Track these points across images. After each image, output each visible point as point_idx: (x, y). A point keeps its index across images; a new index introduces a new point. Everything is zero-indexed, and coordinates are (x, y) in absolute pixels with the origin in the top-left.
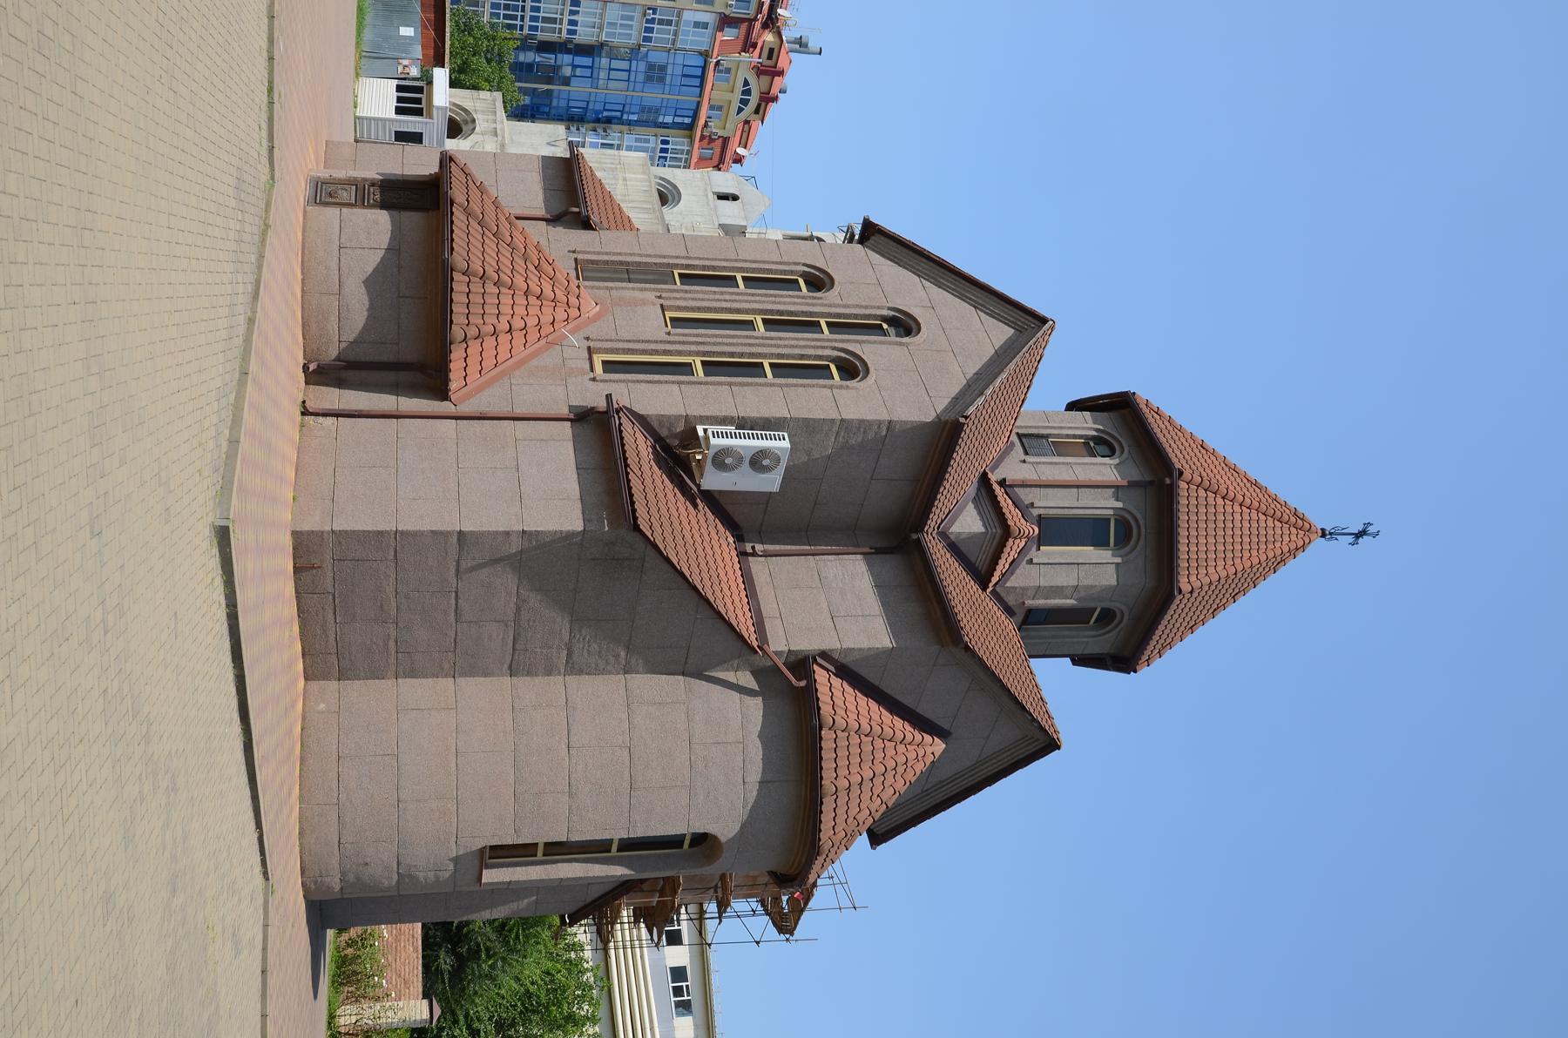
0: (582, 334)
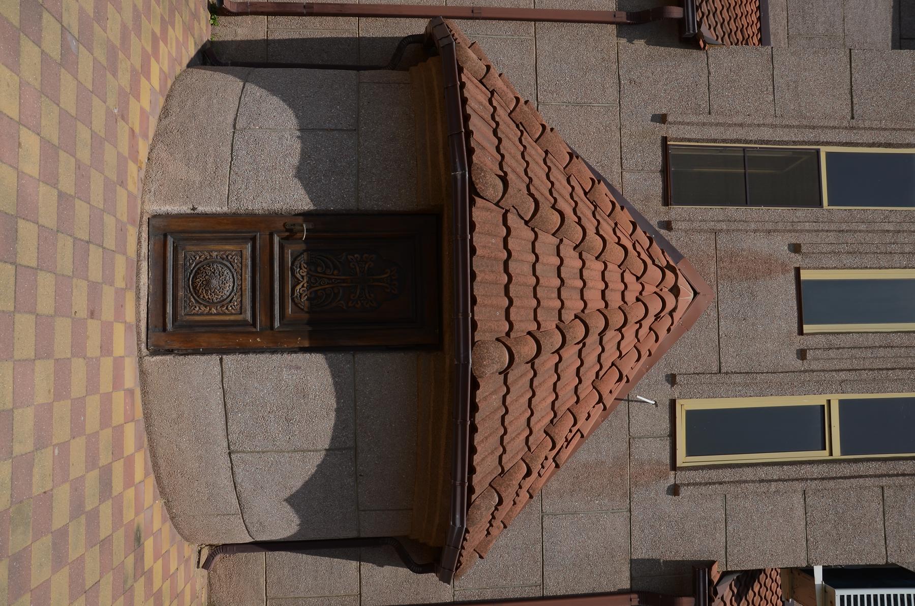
0: (659, 371)
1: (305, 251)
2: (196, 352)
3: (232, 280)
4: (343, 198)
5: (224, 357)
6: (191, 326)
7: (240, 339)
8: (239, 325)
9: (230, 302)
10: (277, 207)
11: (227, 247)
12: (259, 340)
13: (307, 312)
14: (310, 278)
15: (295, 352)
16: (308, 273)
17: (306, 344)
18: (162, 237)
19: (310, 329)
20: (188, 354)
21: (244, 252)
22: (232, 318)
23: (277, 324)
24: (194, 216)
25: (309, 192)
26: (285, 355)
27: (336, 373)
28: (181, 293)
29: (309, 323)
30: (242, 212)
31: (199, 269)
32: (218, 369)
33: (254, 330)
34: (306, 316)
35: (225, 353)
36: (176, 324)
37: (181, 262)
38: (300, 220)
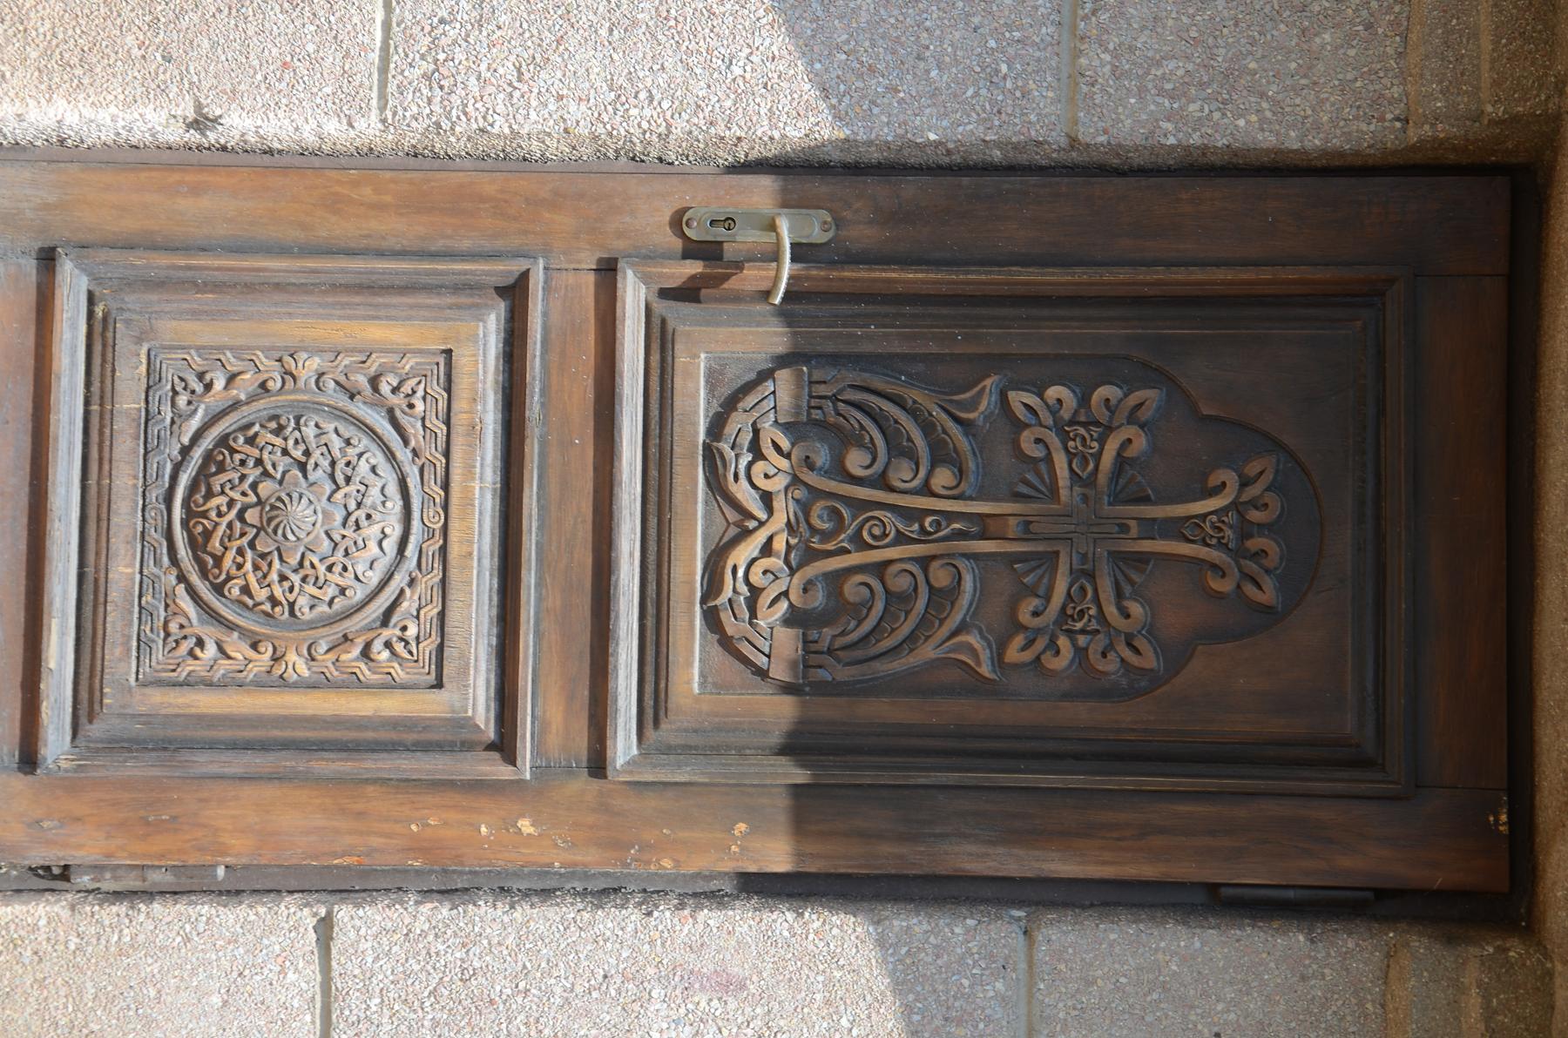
1: (783, 361)
2: (189, 885)
3: (395, 505)
4: (993, 78)
5: (344, 913)
6: (168, 743)
7: (434, 820)
8: (426, 747)
9: (386, 619)
10: (638, 122)
11: (376, 332)
12: (526, 826)
13: (788, 689)
14: (805, 508)
15: (715, 898)
16: (796, 480)
17: (777, 857)
18: (30, 266)
19: (801, 776)
20: (149, 895)
21: (462, 360)
22: (392, 705)
23: (624, 746)
24: (204, 160)
25: (811, 45)
26: (665, 915)
27: (907, 980)
28: (123, 571)
29: (795, 746)
30: (458, 145)
31: (223, 441)
32: (304, 977)
33: (504, 772)
34: (781, 711)
35: (343, 893)
36: (95, 730)
37: (129, 401)
38: (761, 192)
